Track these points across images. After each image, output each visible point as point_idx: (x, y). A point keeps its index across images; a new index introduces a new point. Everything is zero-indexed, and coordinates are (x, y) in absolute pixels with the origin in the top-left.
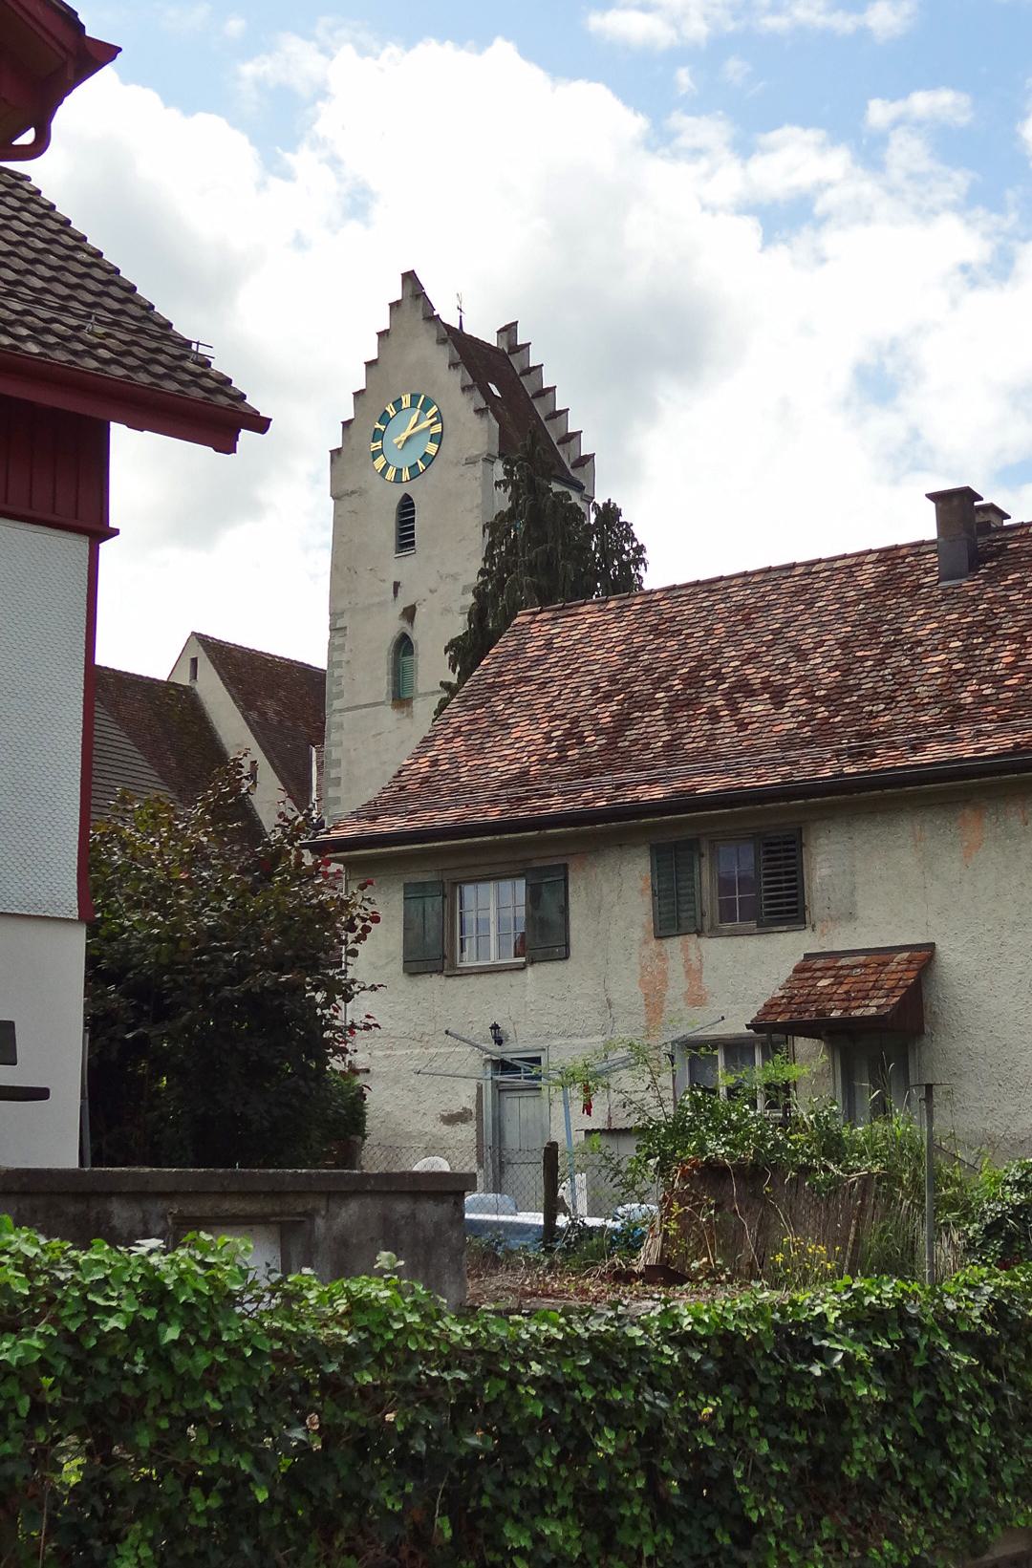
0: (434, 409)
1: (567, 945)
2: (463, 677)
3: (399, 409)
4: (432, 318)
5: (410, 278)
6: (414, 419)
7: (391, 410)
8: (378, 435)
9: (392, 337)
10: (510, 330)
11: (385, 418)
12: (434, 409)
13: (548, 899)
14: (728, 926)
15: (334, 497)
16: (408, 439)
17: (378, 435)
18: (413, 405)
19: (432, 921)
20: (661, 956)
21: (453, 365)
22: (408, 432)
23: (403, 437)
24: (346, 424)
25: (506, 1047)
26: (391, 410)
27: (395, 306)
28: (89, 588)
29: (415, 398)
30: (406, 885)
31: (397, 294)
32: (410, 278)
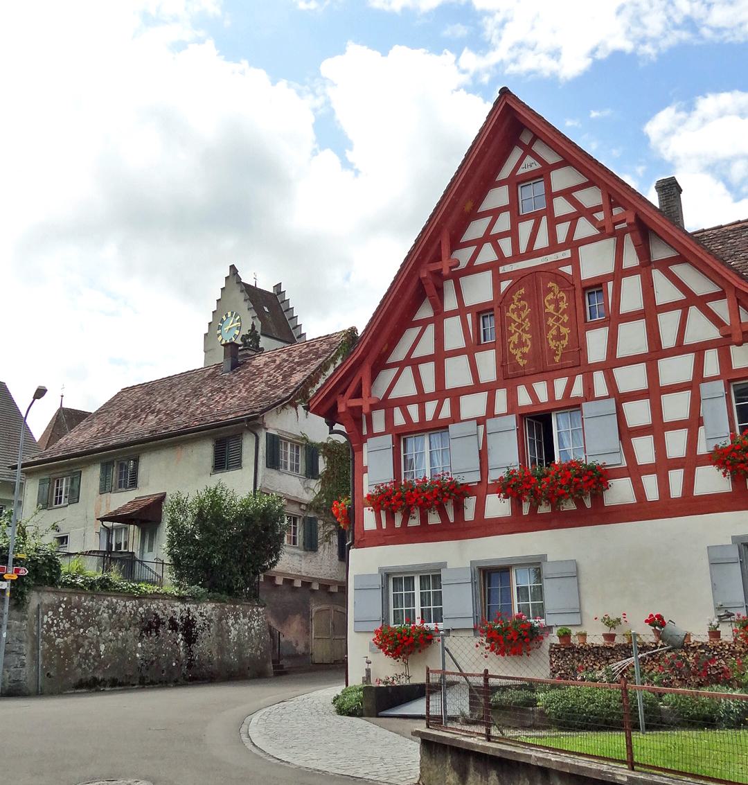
0: (238, 317)
1: (78, 498)
2: (716, 457)
3: (227, 318)
4: (239, 281)
5: (232, 267)
6: (231, 322)
7: (224, 318)
8: (220, 328)
9: (226, 289)
10: (278, 286)
11: (222, 321)
12: (238, 317)
13: (76, 482)
14: (120, 490)
15: (205, 352)
16: (229, 329)
17: (220, 328)
18: (232, 316)
19: (46, 491)
20: (101, 501)
21: (245, 300)
22: (229, 327)
23: (227, 328)
24: (210, 324)
25: (60, 532)
26: (224, 318)
27: (227, 278)
28: (715, 380)
29: (232, 313)
30: (40, 480)
31: (228, 274)
32: (232, 267)
